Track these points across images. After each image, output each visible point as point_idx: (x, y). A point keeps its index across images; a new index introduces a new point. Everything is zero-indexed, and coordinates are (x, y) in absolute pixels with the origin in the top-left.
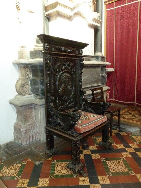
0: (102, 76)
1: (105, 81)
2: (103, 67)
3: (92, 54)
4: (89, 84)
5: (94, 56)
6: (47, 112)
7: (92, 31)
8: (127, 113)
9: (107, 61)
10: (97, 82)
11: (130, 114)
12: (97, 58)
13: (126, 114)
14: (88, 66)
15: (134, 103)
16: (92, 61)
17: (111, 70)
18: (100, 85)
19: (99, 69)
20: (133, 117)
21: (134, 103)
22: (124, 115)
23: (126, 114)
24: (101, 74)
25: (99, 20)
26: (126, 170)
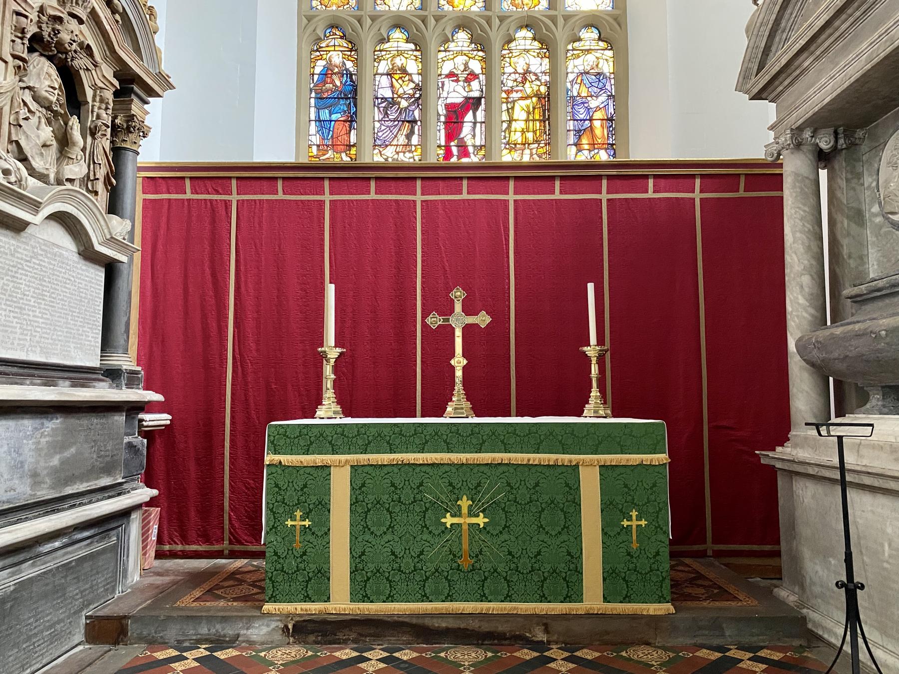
0: (130, 446)
1: (141, 465)
2: (133, 409)
3: (93, 361)
4: (82, 481)
5: (100, 369)
6: (154, 324)
7: (98, 275)
8: (231, 583)
9: (147, 388)
10: (108, 470)
11: (241, 585)
12: (113, 375)
13: (227, 587)
14: (82, 407)
15: (471, 320)
16: (94, 387)
17: (164, 419)
18: (120, 480)
19: (120, 419)
20: (255, 590)
21: (471, 320)
22: (222, 590)
23: (227, 587)
24: (127, 439)
25: (125, 242)
26: (490, 654)
